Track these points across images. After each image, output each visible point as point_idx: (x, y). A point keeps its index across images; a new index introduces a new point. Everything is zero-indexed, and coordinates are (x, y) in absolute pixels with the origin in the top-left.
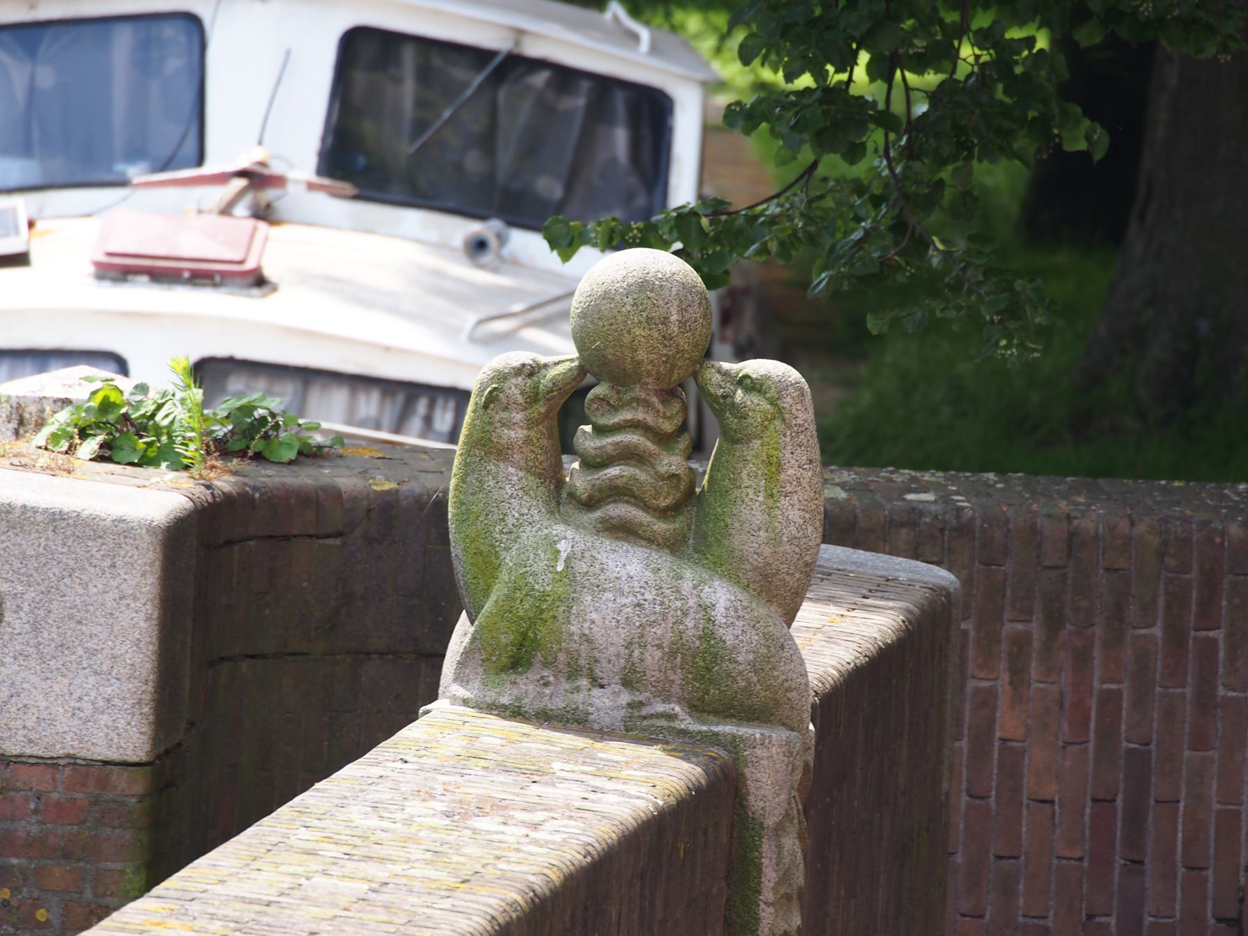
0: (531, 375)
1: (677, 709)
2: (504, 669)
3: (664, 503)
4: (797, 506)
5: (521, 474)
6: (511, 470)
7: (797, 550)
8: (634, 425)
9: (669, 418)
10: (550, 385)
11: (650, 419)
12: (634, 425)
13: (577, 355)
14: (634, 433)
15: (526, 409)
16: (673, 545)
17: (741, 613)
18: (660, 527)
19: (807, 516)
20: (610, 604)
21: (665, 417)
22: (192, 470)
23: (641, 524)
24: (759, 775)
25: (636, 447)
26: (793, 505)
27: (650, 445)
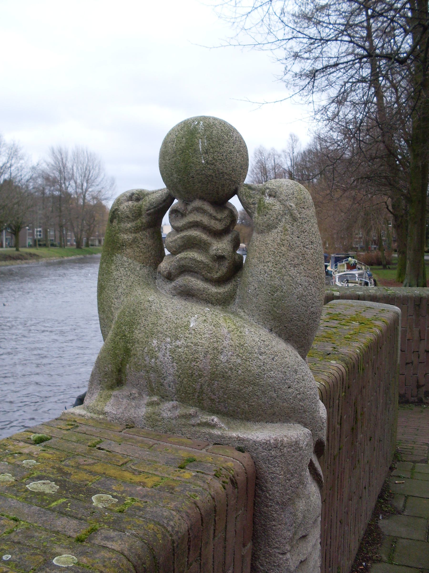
0: (138, 200)
1: (216, 419)
2: (111, 388)
3: (216, 276)
4: (303, 274)
5: (130, 261)
6: (125, 259)
7: (304, 303)
8: (195, 225)
9: (220, 220)
10: (148, 205)
11: (205, 220)
12: (195, 225)
13: (165, 187)
14: (196, 230)
15: (133, 220)
16: (224, 302)
17: (262, 350)
18: (214, 290)
19: (311, 280)
20: (169, 346)
21: (216, 219)
22: (323, 298)
23: (199, 290)
24: (274, 469)
25: (195, 238)
26: (300, 273)
27: (204, 236)
